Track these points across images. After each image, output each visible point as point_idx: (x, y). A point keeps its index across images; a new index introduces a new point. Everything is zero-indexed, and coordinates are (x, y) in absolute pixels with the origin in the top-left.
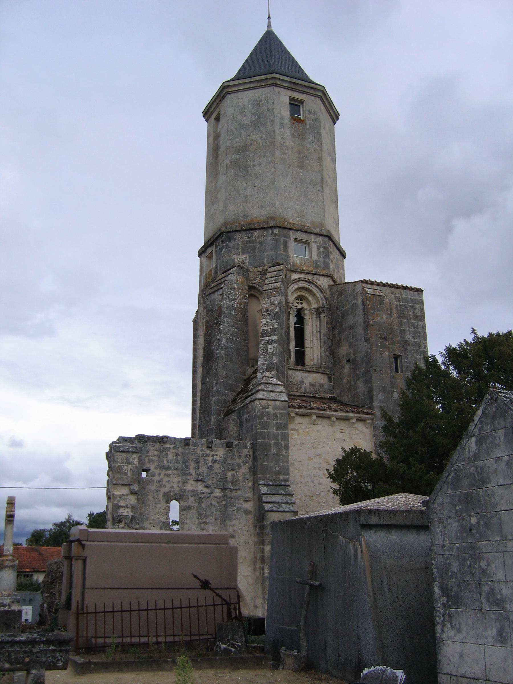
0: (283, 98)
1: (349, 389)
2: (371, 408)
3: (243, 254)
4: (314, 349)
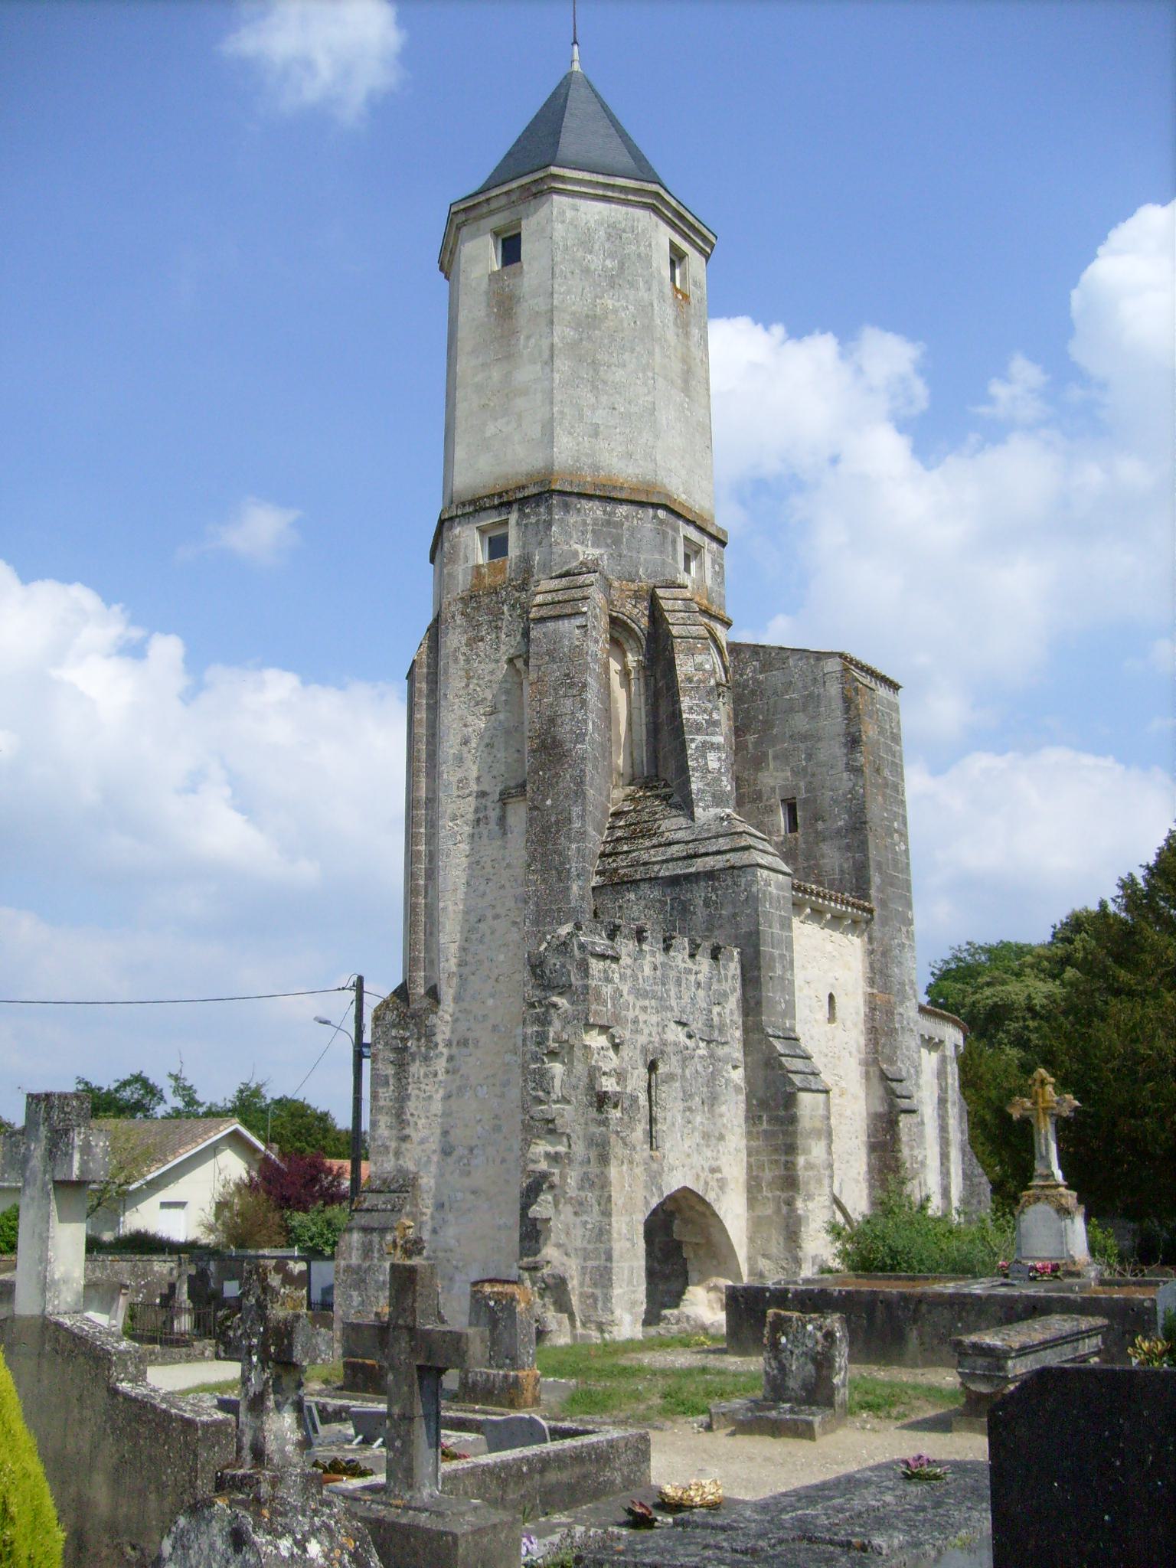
2: (866, 896)
3: (596, 545)
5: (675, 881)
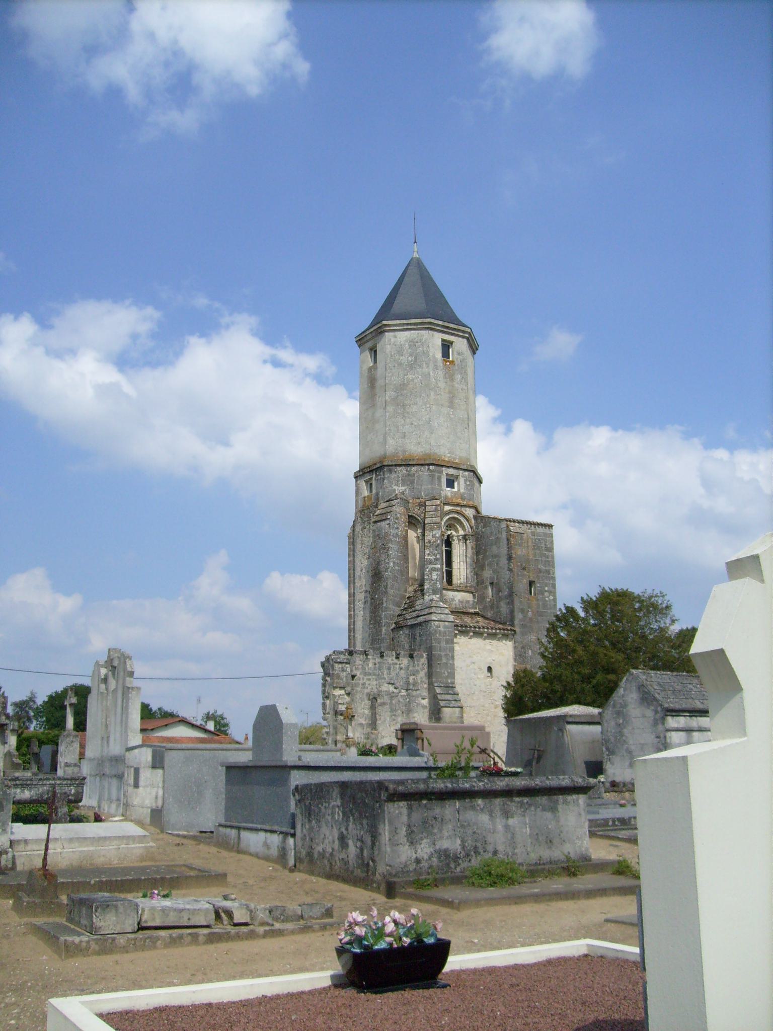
0: (437, 339)
1: (492, 607)
2: (512, 625)
4: (461, 571)
5: (413, 626)
